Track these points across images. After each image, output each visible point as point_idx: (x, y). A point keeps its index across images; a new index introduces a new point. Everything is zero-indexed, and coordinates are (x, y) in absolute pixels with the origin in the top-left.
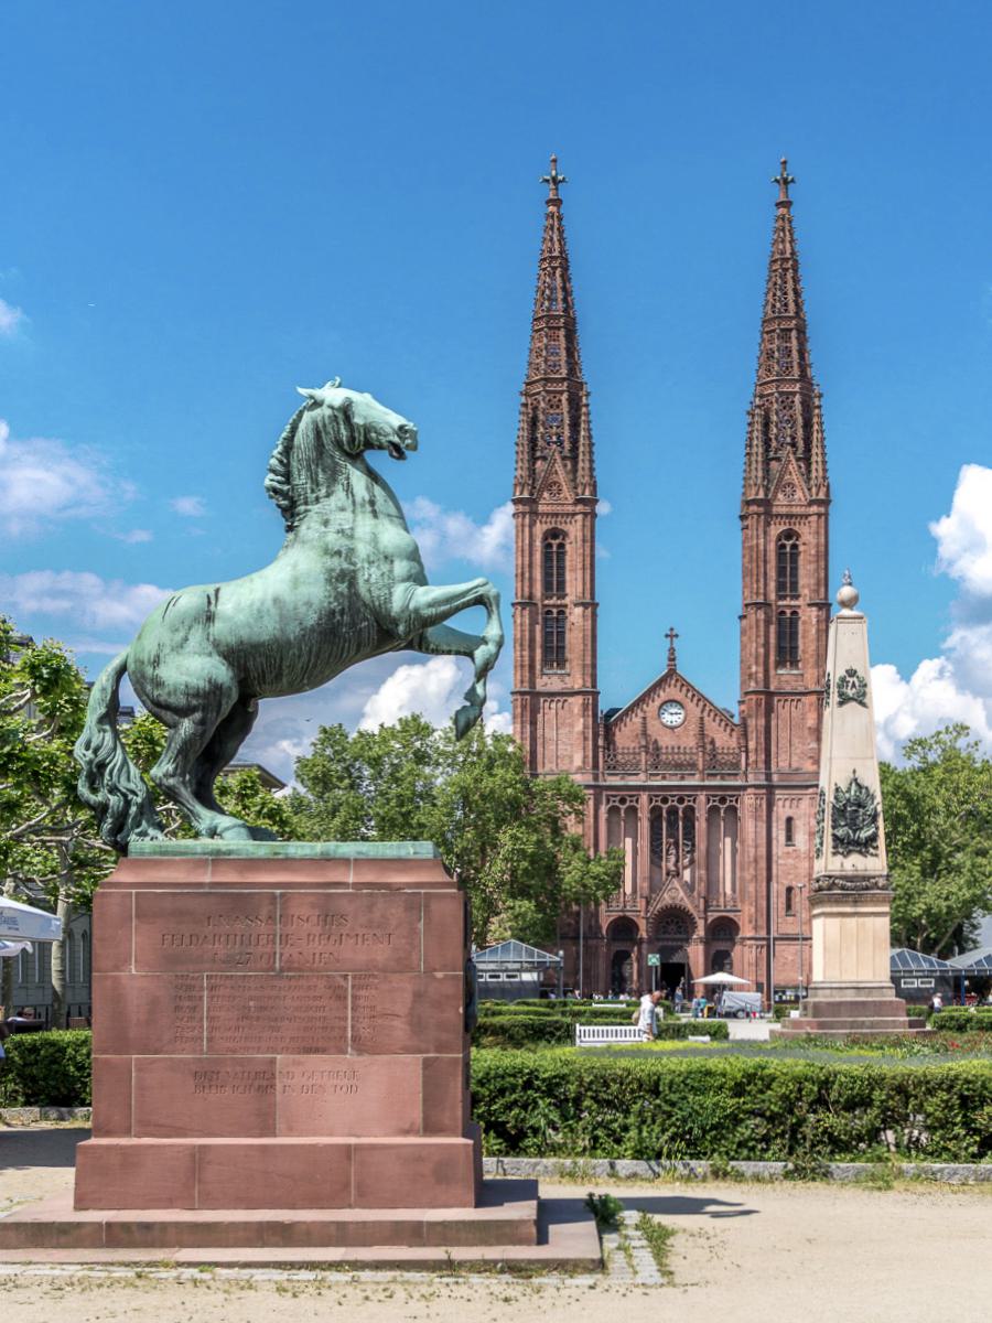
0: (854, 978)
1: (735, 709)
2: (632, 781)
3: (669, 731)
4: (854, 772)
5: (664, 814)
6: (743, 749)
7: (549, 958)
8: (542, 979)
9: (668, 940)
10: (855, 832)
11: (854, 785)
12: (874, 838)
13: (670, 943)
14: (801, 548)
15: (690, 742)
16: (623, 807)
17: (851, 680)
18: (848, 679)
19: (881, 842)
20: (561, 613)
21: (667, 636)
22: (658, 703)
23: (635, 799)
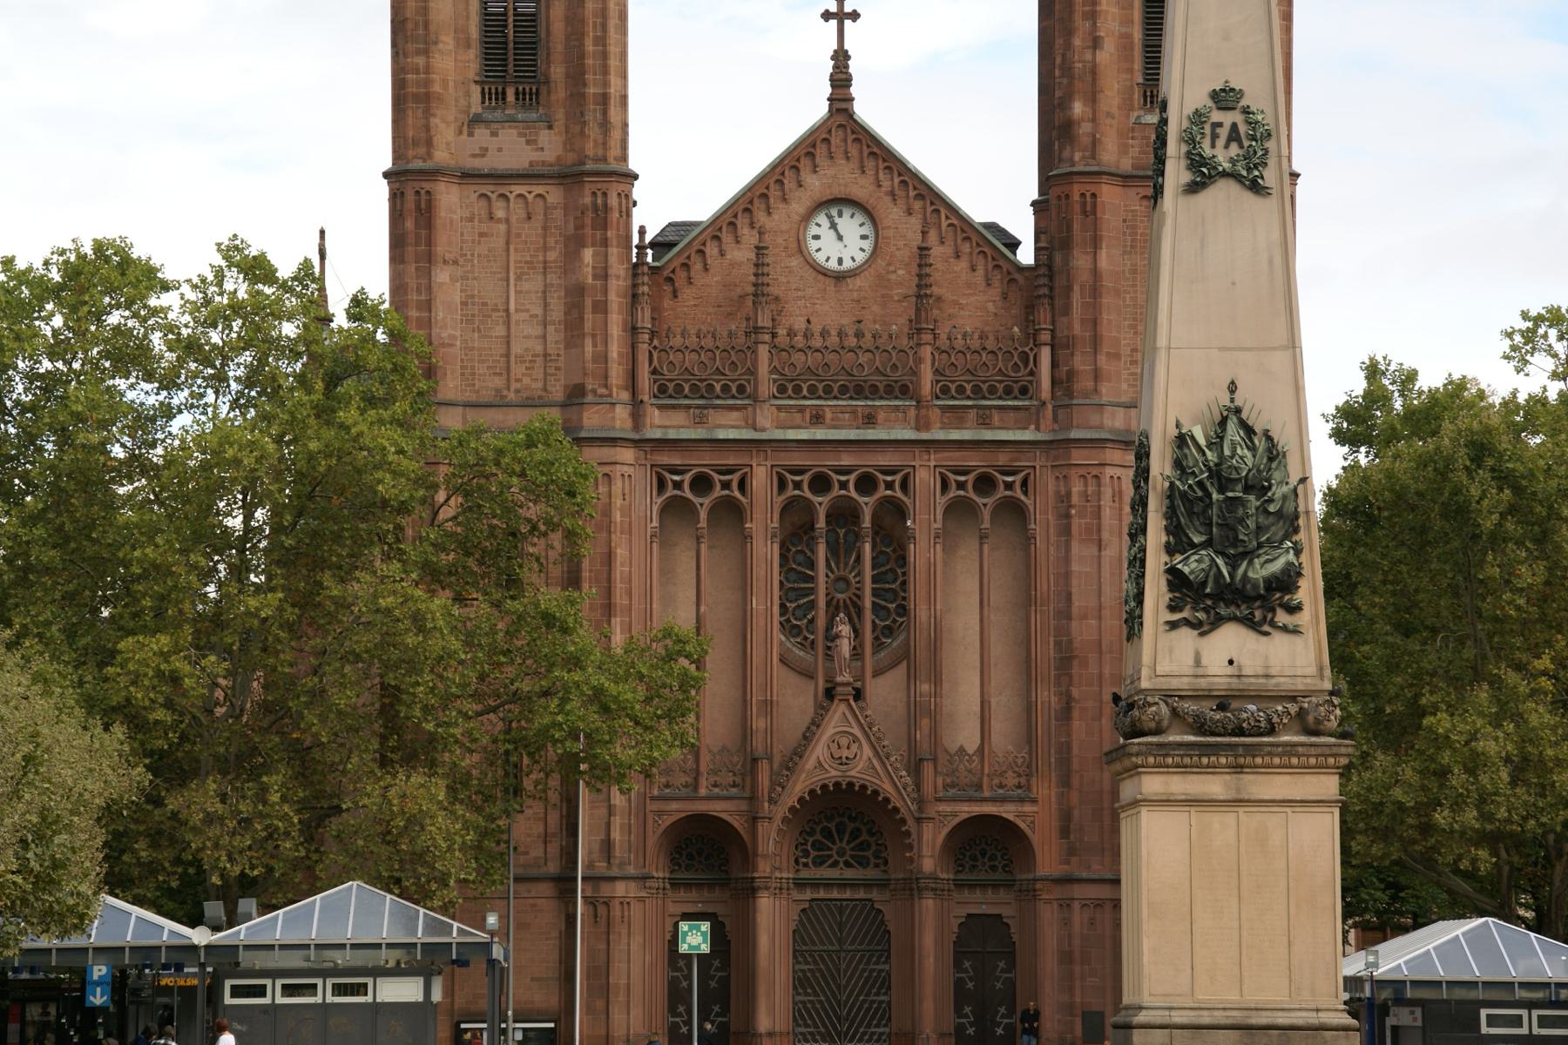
0: (1232, 997)
1: (1022, 226)
2: (728, 427)
4: (1233, 388)
5: (821, 523)
10: (1233, 566)
12: (1286, 582)
16: (704, 504)
17: (1227, 118)
18: (1217, 116)
19: (1310, 591)
22: (798, 207)
23: (735, 478)
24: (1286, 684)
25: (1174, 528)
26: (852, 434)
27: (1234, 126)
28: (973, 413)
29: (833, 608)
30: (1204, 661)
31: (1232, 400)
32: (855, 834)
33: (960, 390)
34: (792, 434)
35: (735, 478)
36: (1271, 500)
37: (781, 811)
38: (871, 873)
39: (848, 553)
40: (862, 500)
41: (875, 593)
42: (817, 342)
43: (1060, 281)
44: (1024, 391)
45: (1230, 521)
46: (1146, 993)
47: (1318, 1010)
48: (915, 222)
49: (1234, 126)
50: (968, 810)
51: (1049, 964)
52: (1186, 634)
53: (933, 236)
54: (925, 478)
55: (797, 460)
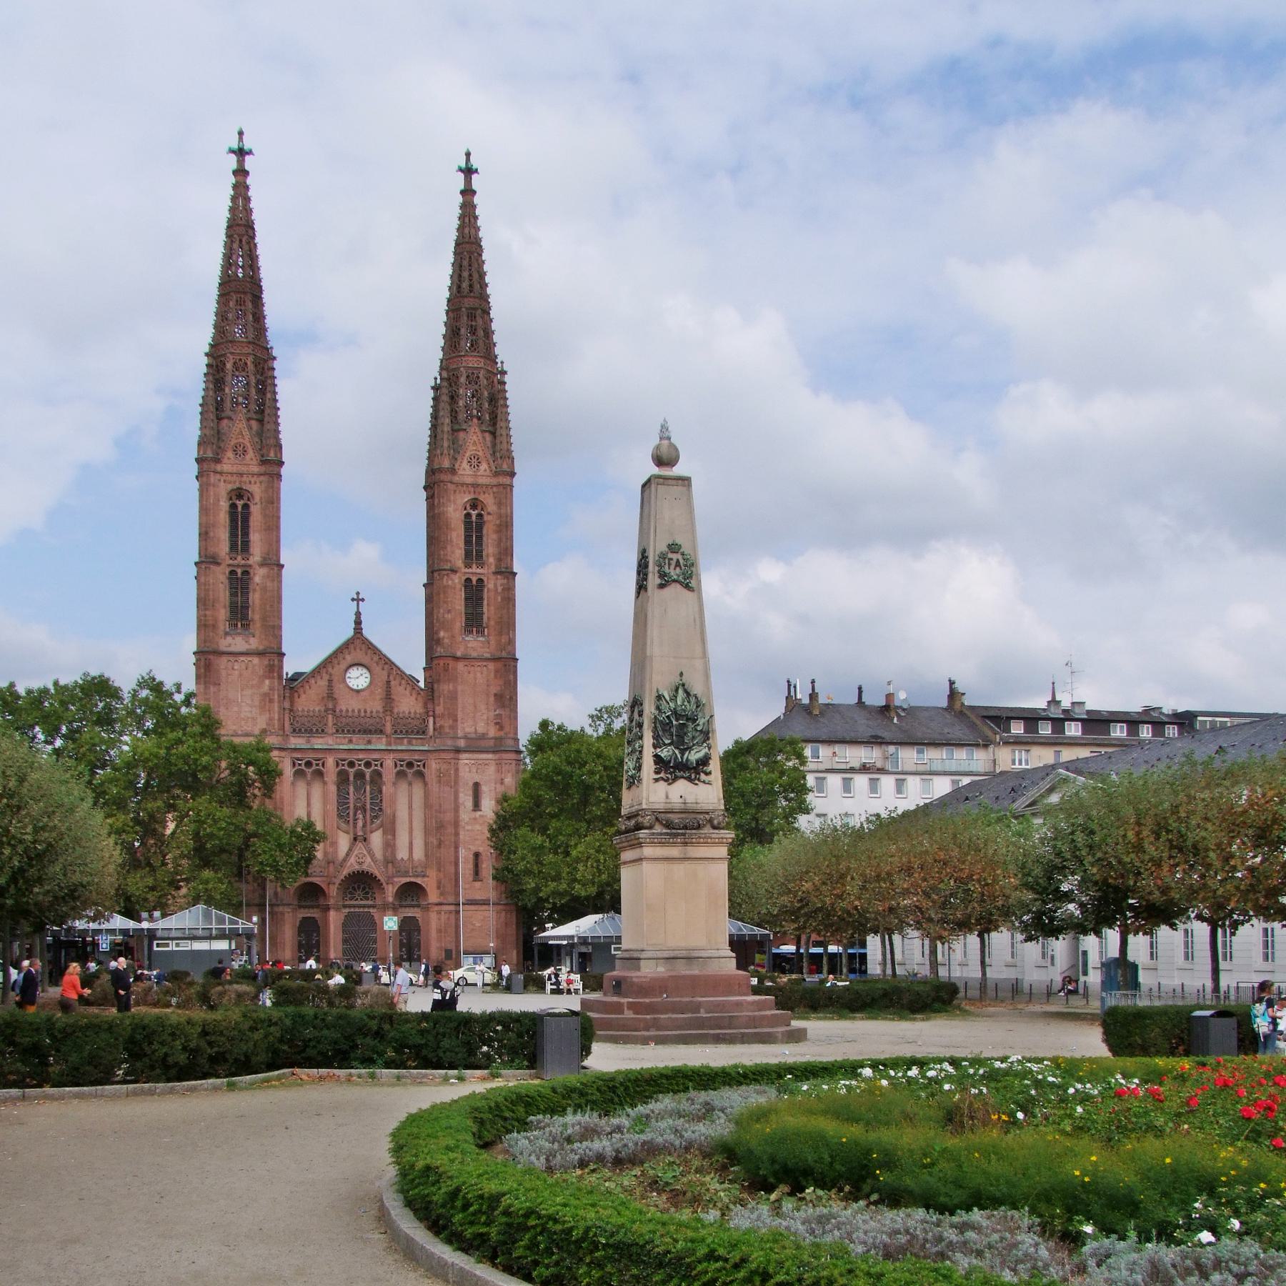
0: (683, 944)
1: (420, 676)
2: (318, 743)
3: (355, 694)
4: (681, 674)
5: (351, 778)
6: (431, 713)
7: (241, 925)
8: (233, 947)
9: (354, 906)
11: (681, 691)
12: (705, 761)
13: (357, 910)
14: (486, 518)
15: (376, 706)
17: (674, 557)
18: (670, 555)
20: (246, 573)
21: (353, 600)
22: (343, 666)
23: (321, 762)
24: (706, 807)
25: (656, 737)
26: (363, 747)
27: (678, 561)
28: (405, 740)
29: (356, 809)
30: (670, 796)
32: (364, 889)
33: (401, 732)
34: (341, 747)
35: (321, 762)
37: (338, 881)
38: (370, 903)
39: (360, 788)
40: (366, 770)
41: (371, 804)
42: (350, 714)
43: (436, 694)
44: (424, 732)
48: (385, 673)
49: (678, 561)
50: (408, 880)
51: (434, 934)
52: (662, 783)
53: (391, 678)
54: (389, 763)
55: (344, 756)
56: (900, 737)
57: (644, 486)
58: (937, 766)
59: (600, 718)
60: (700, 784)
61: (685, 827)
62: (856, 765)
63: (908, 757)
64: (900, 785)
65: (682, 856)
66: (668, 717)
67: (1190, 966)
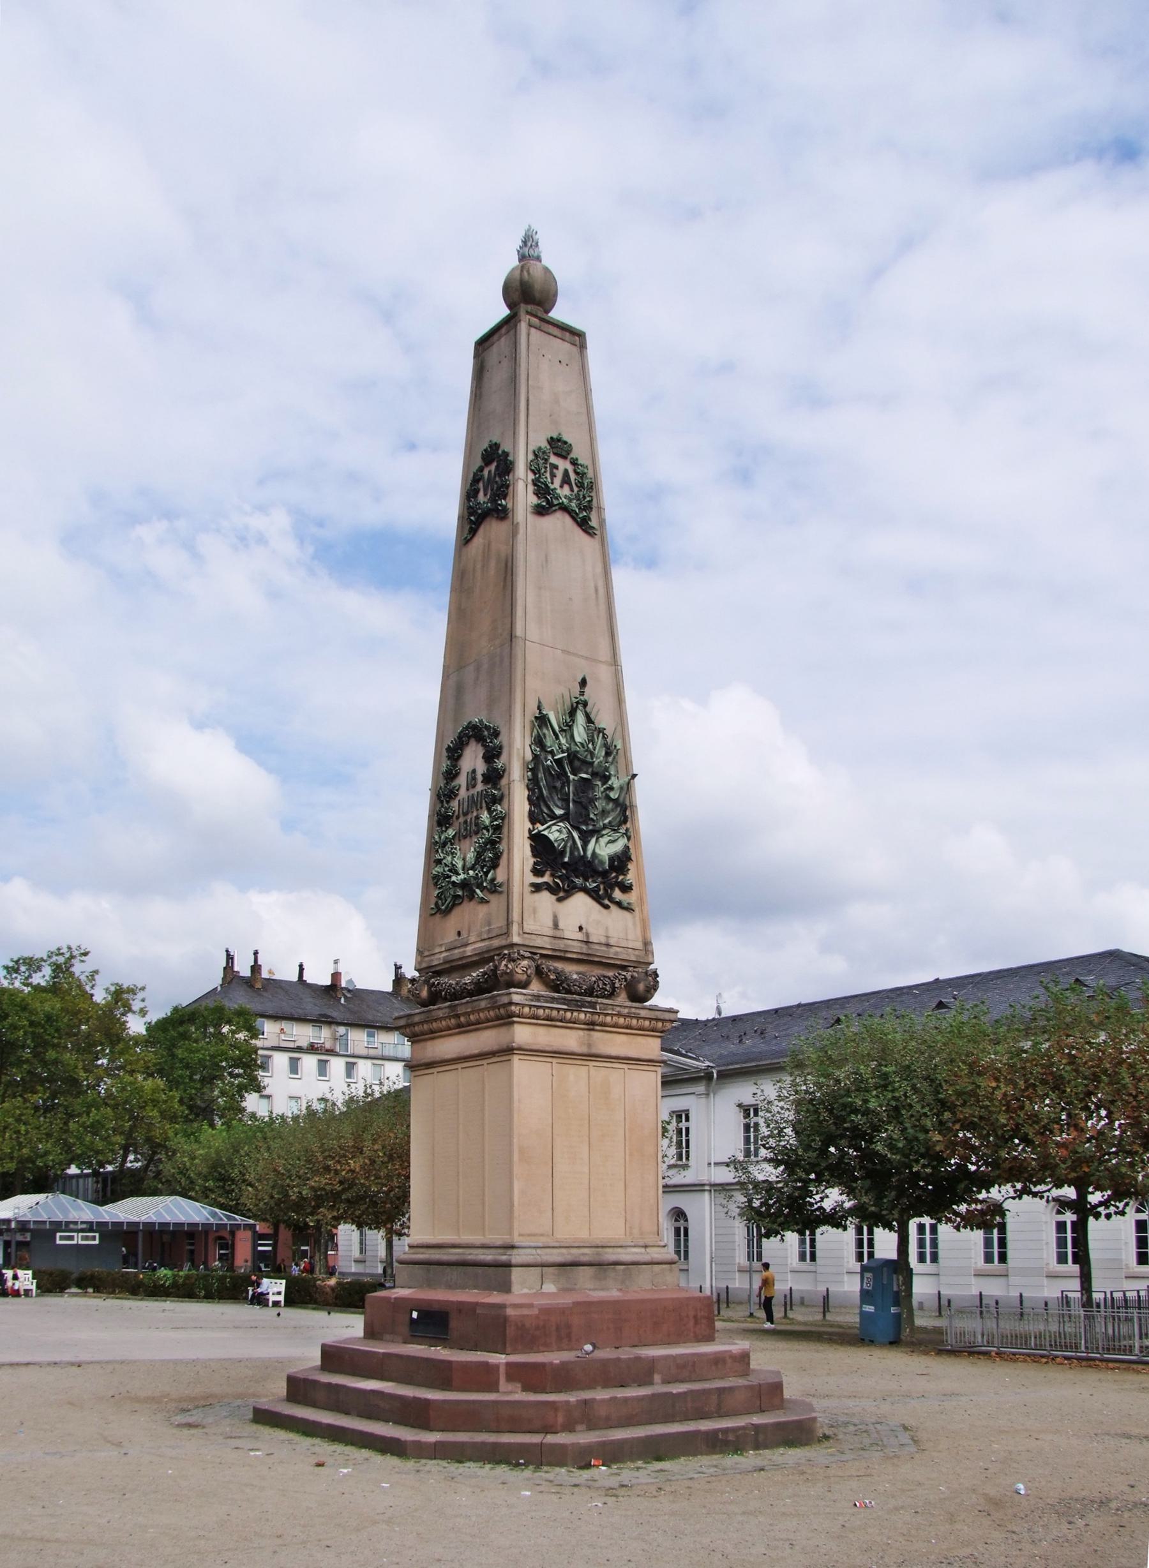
0: (583, 1234)
25: (536, 800)
30: (561, 925)
31: (582, 693)
36: (611, 788)
45: (583, 800)
46: (516, 1233)
47: (646, 1247)
52: (545, 895)
56: (351, 1018)
57: (483, 344)
58: (389, 1051)
59: (17, 971)
60: (613, 908)
61: (590, 992)
62: (304, 1043)
63: (358, 1039)
64: (350, 1068)
65: (584, 1050)
66: (559, 762)
67: (812, 1268)
